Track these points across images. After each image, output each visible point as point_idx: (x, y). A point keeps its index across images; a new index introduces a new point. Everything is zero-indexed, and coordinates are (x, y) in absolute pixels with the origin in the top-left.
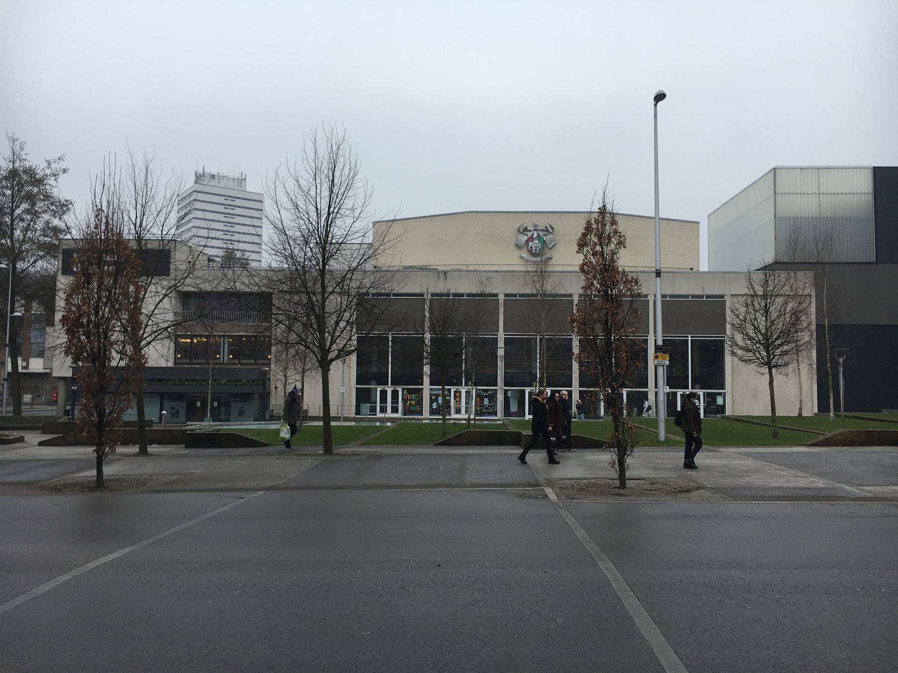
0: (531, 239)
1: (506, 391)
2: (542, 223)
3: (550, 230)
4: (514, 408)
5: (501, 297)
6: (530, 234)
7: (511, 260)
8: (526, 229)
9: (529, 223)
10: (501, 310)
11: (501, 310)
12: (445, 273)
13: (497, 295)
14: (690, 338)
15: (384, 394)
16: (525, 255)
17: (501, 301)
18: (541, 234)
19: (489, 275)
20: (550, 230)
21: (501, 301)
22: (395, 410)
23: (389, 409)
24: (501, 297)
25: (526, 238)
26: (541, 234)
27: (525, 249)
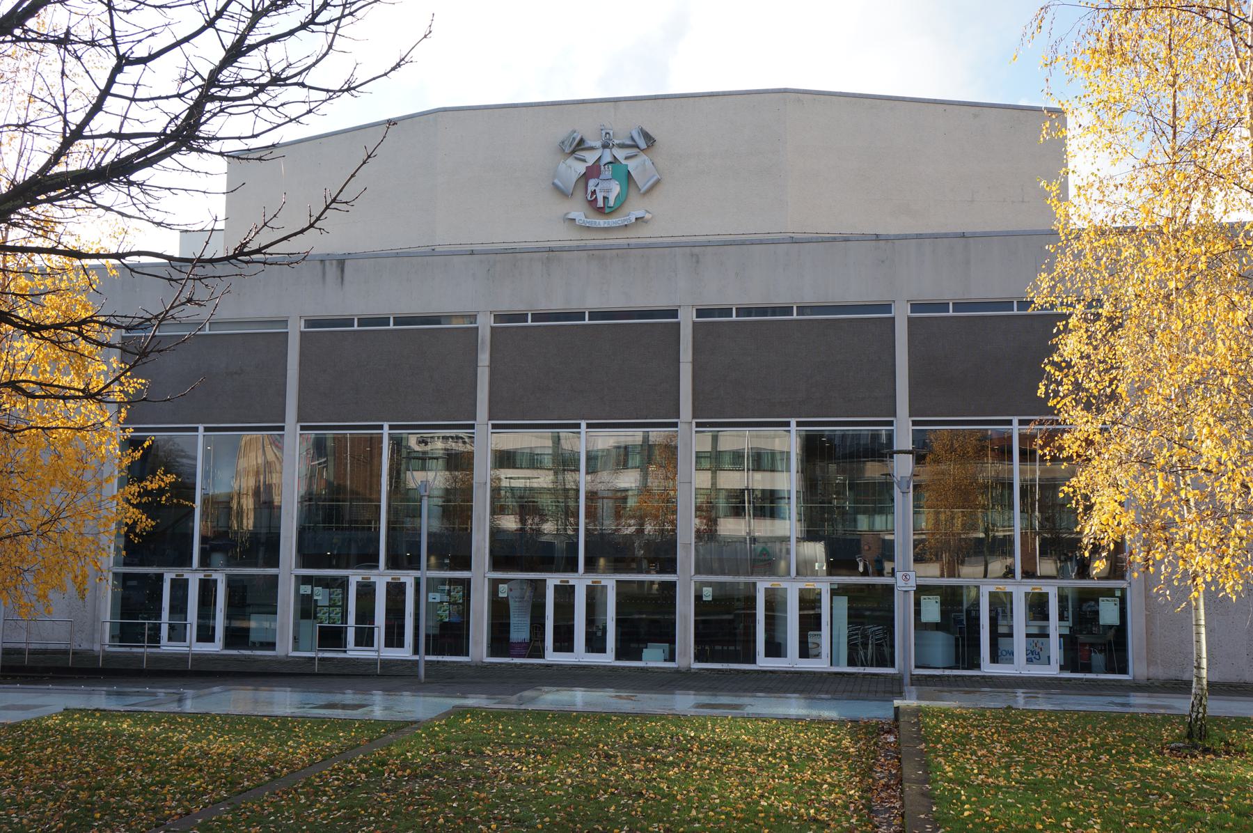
0: (593, 171)
1: (495, 583)
2: (624, 127)
3: (642, 144)
4: (519, 631)
5: (687, 319)
6: (591, 158)
7: (543, 222)
8: (580, 145)
9: (588, 129)
10: (484, 358)
11: (484, 358)
12: (341, 263)
13: (673, 313)
14: (386, 432)
15: (180, 586)
16: (579, 213)
17: (485, 335)
18: (620, 154)
19: (696, 250)
20: (642, 144)
21: (485, 335)
22: (206, 634)
23: (192, 632)
24: (687, 319)
25: (581, 168)
26: (620, 154)
27: (579, 195)
